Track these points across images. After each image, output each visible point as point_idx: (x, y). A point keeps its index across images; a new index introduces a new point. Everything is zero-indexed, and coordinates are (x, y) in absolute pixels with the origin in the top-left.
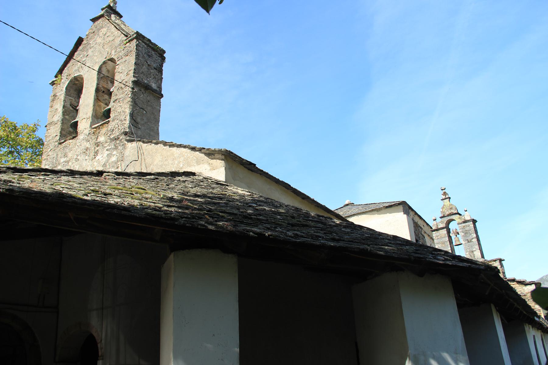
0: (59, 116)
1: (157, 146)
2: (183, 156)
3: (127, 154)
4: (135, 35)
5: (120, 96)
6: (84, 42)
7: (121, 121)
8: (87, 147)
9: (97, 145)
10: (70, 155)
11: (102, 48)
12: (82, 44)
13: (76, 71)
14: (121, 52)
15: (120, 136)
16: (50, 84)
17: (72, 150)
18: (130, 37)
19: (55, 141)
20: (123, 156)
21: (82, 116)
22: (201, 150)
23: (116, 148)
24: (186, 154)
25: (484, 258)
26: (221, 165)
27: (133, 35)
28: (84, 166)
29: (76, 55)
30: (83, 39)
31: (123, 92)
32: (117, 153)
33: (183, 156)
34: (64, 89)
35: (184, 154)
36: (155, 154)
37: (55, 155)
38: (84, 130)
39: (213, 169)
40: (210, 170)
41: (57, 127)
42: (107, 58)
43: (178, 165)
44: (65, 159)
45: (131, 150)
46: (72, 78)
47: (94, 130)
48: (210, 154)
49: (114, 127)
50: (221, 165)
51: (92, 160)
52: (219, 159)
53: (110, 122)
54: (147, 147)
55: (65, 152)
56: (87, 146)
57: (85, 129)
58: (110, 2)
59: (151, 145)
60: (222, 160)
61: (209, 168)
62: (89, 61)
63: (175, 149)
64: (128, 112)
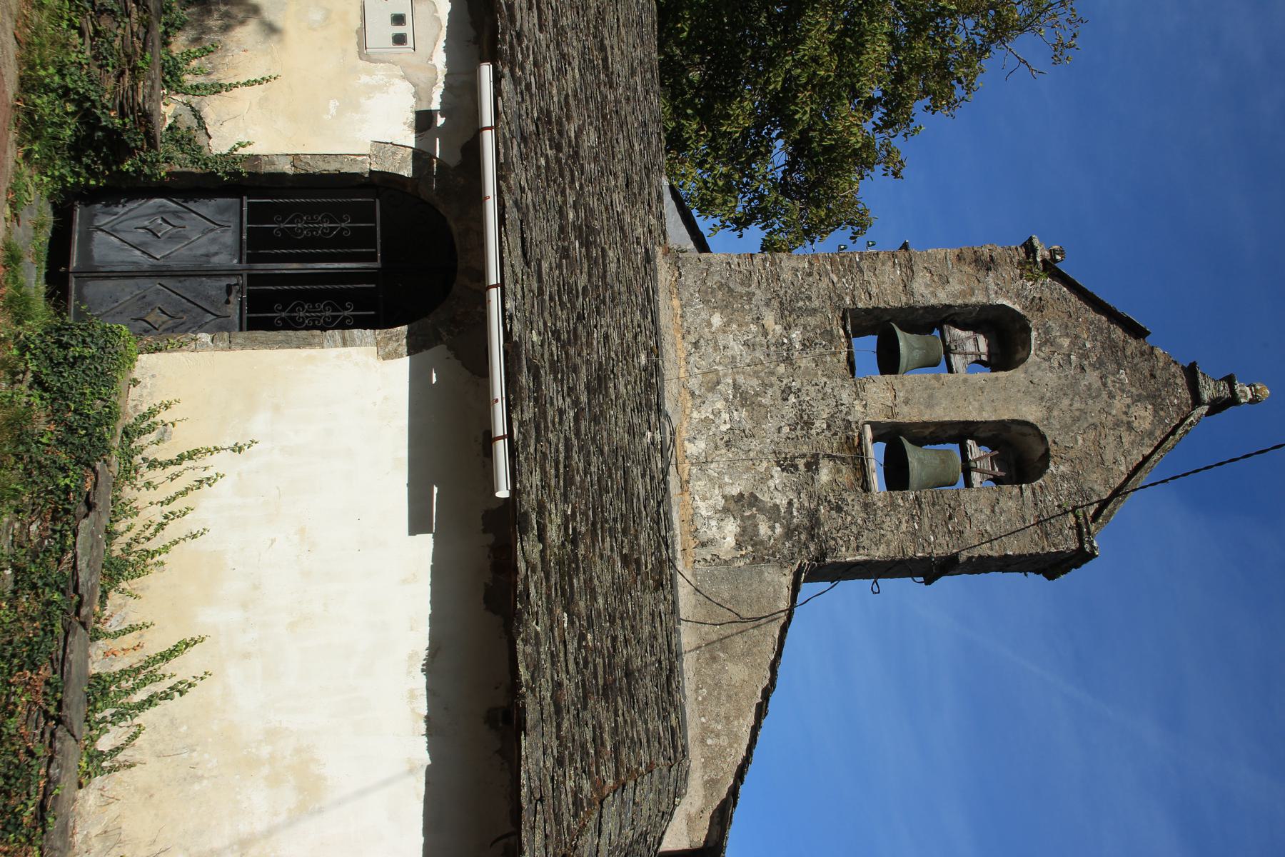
0: (923, 297)
1: (767, 667)
2: (731, 746)
3: (766, 574)
4: (1088, 550)
5: (926, 519)
6: (1133, 344)
7: (859, 532)
8: (813, 424)
9: (812, 466)
10: (805, 362)
11: (1091, 421)
12: (1130, 335)
13: (1047, 331)
14: (1057, 497)
15: (816, 544)
16: (1031, 239)
17: (817, 365)
18: (1089, 533)
19: (856, 293)
20: (763, 559)
21: (903, 385)
22: (734, 793)
23: (789, 533)
24: (733, 751)
25: (804, 582)
26: (696, 840)
27: (1091, 543)
28: (763, 426)
29: (1100, 320)
30: (1144, 339)
31: (936, 526)
32: (774, 540)
33: (731, 746)
34: (1001, 301)
35: (735, 745)
36: (749, 665)
37: (816, 303)
38: (864, 402)
39: (690, 821)
40: (689, 816)
41: (894, 294)
42: (1053, 448)
43: (712, 732)
44: (798, 346)
45: (774, 587)
46: (1030, 319)
47: (856, 439)
48: (722, 817)
49: (847, 513)
50: (696, 840)
51: (775, 452)
52: (708, 836)
53: (864, 495)
54: (770, 640)
55: (817, 341)
56: (817, 424)
57: (866, 404)
58: (1256, 390)
59: (774, 649)
60: (706, 842)
61: (693, 811)
62: (1063, 381)
63: (750, 719)
64: (878, 555)
